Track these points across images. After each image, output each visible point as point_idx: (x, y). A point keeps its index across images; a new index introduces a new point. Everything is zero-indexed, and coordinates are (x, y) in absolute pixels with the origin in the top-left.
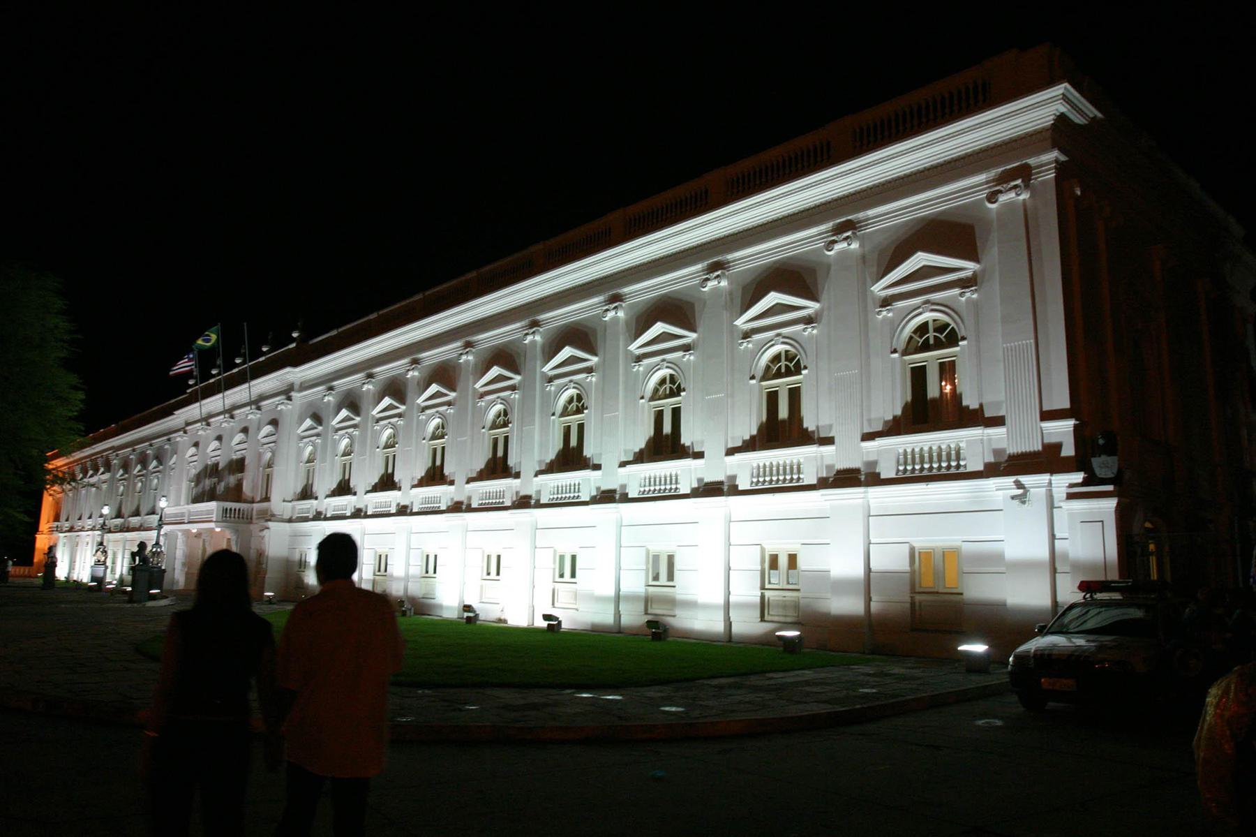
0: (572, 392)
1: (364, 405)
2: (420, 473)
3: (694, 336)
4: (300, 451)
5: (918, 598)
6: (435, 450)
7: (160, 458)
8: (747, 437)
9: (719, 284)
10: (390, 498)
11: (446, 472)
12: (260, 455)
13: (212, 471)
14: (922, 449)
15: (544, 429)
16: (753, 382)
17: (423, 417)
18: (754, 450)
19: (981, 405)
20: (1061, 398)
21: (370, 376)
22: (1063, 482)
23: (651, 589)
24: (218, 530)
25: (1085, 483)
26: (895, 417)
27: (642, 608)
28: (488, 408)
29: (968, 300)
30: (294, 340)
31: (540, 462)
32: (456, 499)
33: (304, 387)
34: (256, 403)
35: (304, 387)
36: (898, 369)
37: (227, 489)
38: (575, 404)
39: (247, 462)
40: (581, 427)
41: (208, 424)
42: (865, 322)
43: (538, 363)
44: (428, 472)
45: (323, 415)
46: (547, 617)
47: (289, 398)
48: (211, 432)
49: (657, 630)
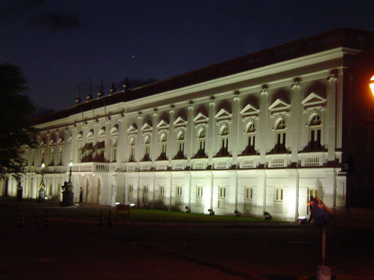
0: (314, 114)
1: (154, 122)
2: (175, 154)
3: (326, 100)
4: (128, 140)
5: (246, 201)
6: (279, 135)
7: (63, 137)
8: (271, 149)
9: (265, 93)
10: (164, 163)
11: (256, 149)
12: (111, 141)
13: (89, 146)
14: (314, 157)
15: (194, 141)
16: (273, 130)
17: (176, 130)
18: (218, 157)
19: (324, 145)
20: (340, 146)
21: (156, 110)
22: (338, 170)
23: (246, 201)
24: (94, 175)
25: (342, 171)
26: (306, 147)
27: (243, 208)
28: (220, 126)
29: (323, 111)
30: (123, 88)
31: (193, 154)
32: (233, 164)
33: (130, 110)
34: (109, 116)
35: (130, 110)
36: (177, 144)
37: (97, 156)
38: (282, 124)
39: (105, 144)
40: (319, 132)
41: (86, 123)
42: (301, 112)
43: (239, 110)
44: (276, 146)
45: (138, 124)
46: (209, 210)
47: (123, 116)
48: (100, 125)
49: (248, 215)
